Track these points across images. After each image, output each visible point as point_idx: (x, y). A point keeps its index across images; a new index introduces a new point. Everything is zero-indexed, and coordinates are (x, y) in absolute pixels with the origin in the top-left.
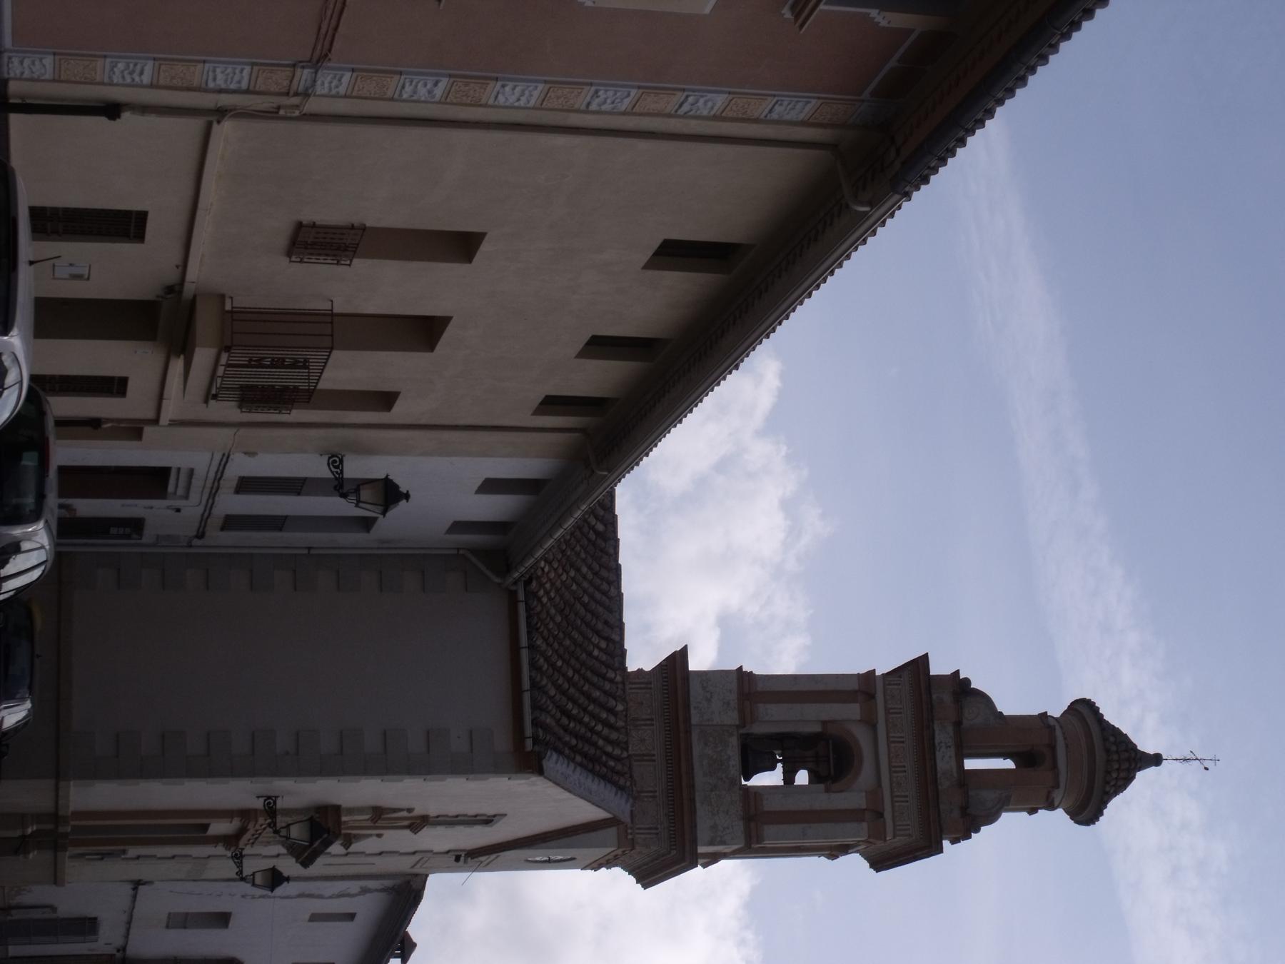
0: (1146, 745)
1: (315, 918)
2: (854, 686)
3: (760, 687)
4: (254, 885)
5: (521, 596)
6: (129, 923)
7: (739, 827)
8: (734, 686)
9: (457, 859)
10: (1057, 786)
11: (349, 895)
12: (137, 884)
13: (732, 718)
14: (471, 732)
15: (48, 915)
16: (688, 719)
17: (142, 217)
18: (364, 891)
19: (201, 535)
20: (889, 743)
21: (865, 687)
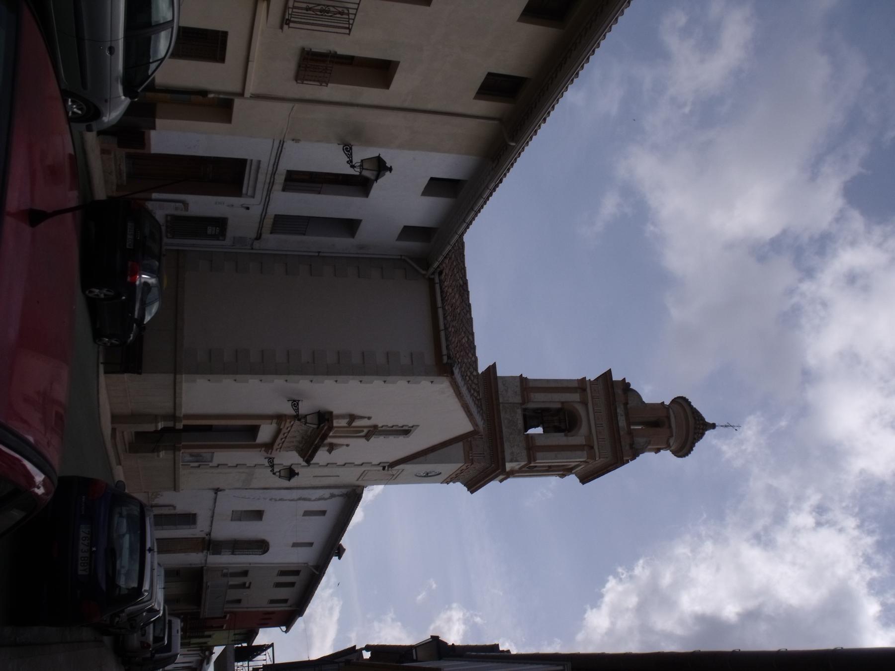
0: (709, 420)
1: (307, 513)
2: (576, 385)
3: (531, 385)
4: (280, 477)
5: (437, 280)
6: (213, 517)
7: (524, 453)
8: (518, 384)
9: (384, 468)
10: (672, 436)
11: (325, 499)
12: (217, 490)
13: (518, 399)
14: (412, 354)
15: (172, 512)
16: (498, 399)
17: (195, 515)
18: (333, 496)
19: (259, 237)
20: (594, 413)
21: (581, 385)
